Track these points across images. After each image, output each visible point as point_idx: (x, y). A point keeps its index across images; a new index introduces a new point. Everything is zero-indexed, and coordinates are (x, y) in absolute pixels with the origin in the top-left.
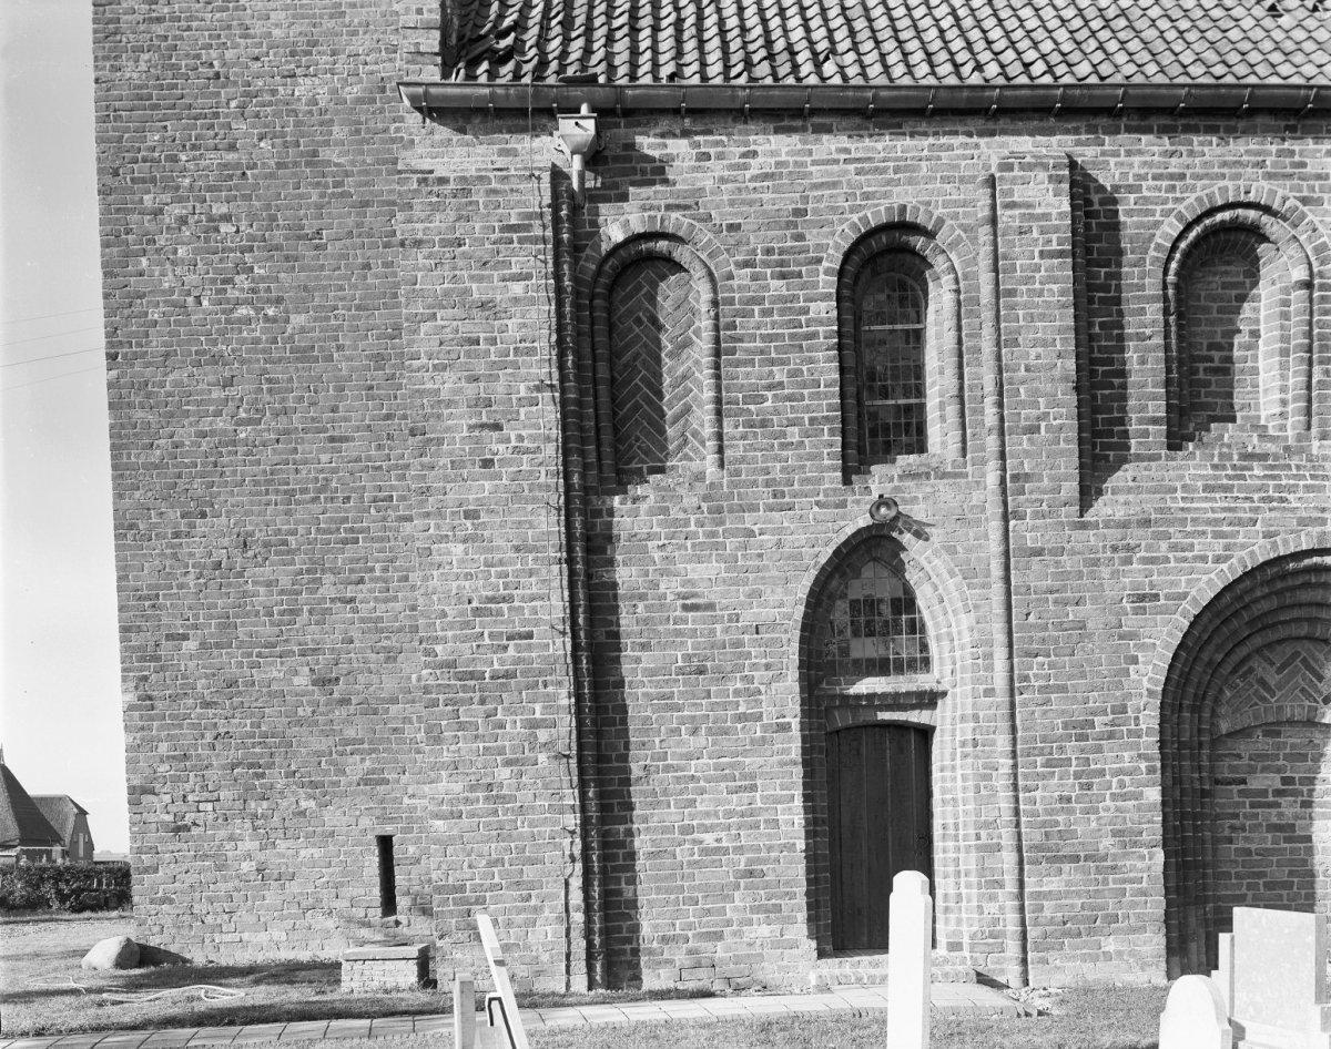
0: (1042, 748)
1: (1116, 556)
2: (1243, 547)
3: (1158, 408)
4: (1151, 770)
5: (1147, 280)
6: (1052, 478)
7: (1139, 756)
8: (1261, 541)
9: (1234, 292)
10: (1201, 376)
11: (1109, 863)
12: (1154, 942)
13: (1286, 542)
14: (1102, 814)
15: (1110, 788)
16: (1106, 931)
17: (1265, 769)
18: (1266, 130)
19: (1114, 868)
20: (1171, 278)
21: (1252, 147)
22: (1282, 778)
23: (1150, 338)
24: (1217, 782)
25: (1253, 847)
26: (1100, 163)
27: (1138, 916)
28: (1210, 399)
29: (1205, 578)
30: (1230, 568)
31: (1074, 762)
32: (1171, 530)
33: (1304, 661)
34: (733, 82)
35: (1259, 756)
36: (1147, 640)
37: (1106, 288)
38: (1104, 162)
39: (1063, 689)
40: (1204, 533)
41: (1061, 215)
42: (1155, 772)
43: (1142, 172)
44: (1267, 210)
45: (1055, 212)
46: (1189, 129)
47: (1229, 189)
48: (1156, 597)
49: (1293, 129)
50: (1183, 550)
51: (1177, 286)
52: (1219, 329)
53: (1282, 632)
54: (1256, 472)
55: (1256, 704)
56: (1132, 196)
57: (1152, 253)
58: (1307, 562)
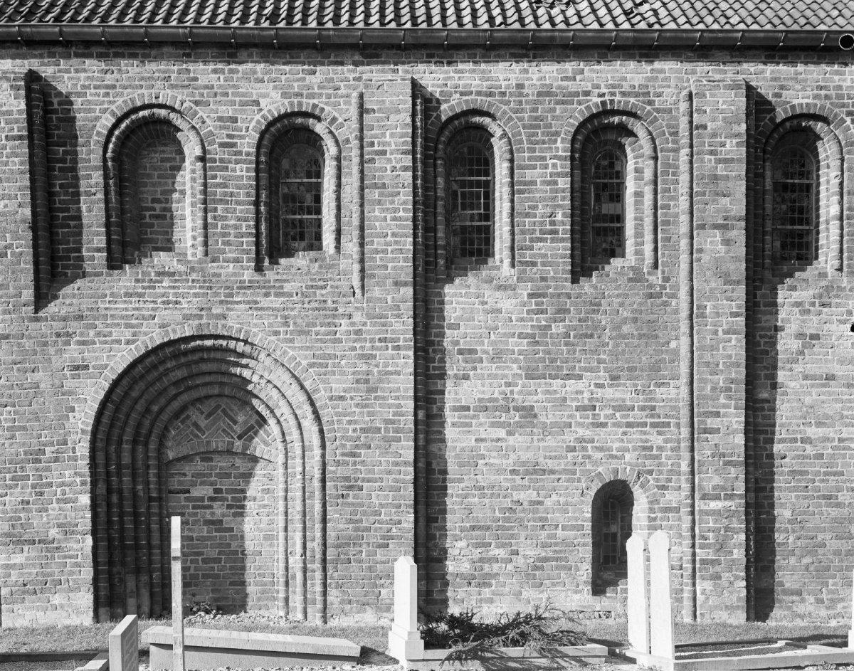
0: (10, 468)
1: (59, 339)
2: (145, 334)
3: (101, 242)
4: (83, 483)
5: (92, 156)
6: (15, 288)
7: (76, 473)
8: (158, 330)
9: (169, 165)
10: (147, 220)
11: (55, 545)
12: (85, 599)
13: (174, 331)
14: (51, 512)
15: (56, 495)
16: (53, 591)
17: (202, 483)
18: (170, 57)
19: (58, 548)
20: (109, 154)
21: (161, 67)
22: (214, 489)
23: (95, 194)
24: (171, 492)
25: (194, 535)
26: (58, 78)
27: (74, 581)
28: (154, 236)
29: (119, 354)
30: (136, 348)
31: (31, 478)
32: (97, 322)
33: (224, 411)
34: (388, 27)
35: (198, 474)
36: (81, 396)
37: (63, 161)
38: (60, 77)
39: (24, 428)
40: (118, 324)
41: (19, 112)
42: (86, 484)
43: (86, 83)
44: (173, 109)
45: (15, 109)
46: (117, 55)
47: (145, 96)
48: (87, 367)
49: (189, 56)
50: (105, 336)
51: (113, 159)
52: (159, 189)
53: (203, 392)
54: (164, 284)
55: (192, 440)
56: (80, 100)
57: (95, 138)
58: (193, 344)
